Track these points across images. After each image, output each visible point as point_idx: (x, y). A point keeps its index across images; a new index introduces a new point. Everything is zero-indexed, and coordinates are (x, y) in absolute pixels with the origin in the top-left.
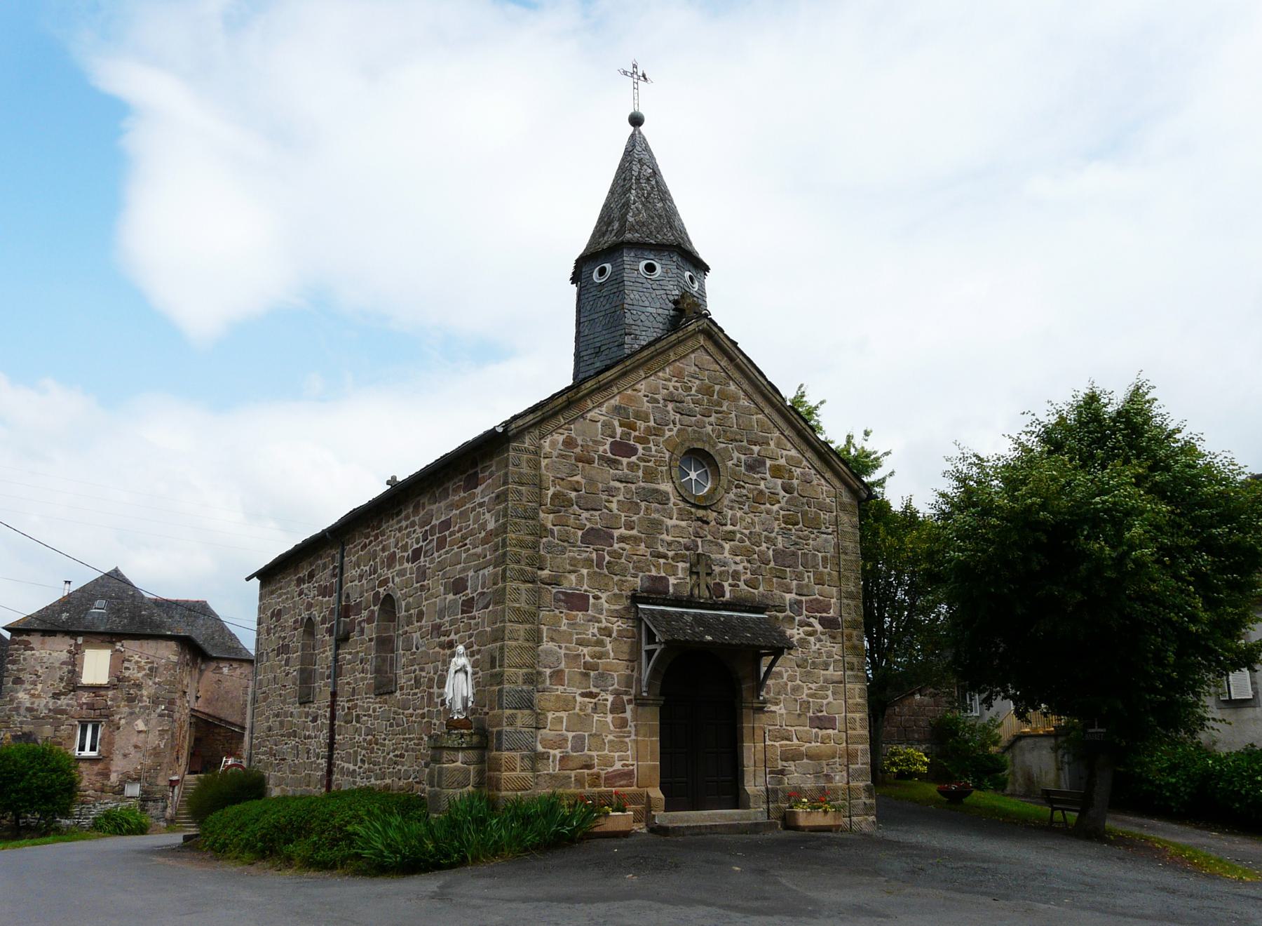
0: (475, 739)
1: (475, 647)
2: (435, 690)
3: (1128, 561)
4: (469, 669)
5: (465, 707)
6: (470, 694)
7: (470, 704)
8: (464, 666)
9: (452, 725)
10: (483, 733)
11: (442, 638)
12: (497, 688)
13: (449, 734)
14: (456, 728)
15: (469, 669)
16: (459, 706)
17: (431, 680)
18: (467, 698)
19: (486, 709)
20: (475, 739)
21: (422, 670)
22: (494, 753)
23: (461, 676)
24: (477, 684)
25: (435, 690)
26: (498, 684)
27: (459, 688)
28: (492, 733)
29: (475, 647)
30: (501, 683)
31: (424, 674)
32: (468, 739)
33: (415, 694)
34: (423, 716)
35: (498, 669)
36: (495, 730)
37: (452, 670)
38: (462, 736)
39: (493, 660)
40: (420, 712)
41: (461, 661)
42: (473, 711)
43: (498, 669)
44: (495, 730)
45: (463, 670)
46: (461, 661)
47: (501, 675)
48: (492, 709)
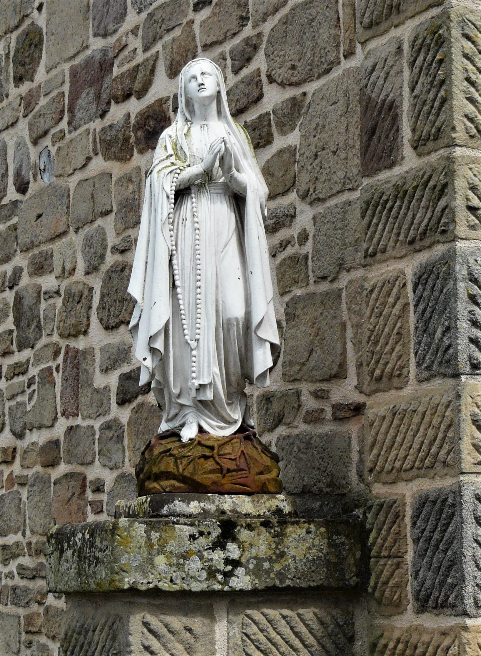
0: (303, 545)
1: (273, 98)
2: (97, 338)
3: (226, 570)
4: (251, 177)
5: (240, 378)
6: (266, 310)
7: (262, 359)
8: (225, 159)
9: (165, 474)
10: (338, 510)
11: (117, 113)
12: (409, 267)
13: (155, 516)
14: (195, 488)
15: (251, 177)
16: (206, 369)
17: (77, 298)
18: (247, 328)
19: (346, 391)
20: (303, 545)
21: (40, 268)
22: (407, 620)
23: (211, 212)
24: (288, 272)
25: (97, 338)
26: (414, 244)
27: (203, 276)
28: (391, 509)
29: (273, 98)
30: (440, 228)
31: (48, 282)
32: (261, 543)
33: (20, 369)
34: (50, 454)
35: (410, 162)
36: (408, 492)
37: (161, 183)
38: (228, 529)
39: (377, 139)
40: (38, 438)
41: (204, 137)
42: (277, 409)
43: (410, 162)
44: (408, 492)
45: (216, 180)
46: (204, 137)
47: (438, 186)
48: (389, 380)
